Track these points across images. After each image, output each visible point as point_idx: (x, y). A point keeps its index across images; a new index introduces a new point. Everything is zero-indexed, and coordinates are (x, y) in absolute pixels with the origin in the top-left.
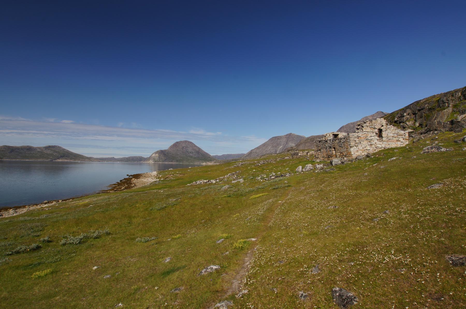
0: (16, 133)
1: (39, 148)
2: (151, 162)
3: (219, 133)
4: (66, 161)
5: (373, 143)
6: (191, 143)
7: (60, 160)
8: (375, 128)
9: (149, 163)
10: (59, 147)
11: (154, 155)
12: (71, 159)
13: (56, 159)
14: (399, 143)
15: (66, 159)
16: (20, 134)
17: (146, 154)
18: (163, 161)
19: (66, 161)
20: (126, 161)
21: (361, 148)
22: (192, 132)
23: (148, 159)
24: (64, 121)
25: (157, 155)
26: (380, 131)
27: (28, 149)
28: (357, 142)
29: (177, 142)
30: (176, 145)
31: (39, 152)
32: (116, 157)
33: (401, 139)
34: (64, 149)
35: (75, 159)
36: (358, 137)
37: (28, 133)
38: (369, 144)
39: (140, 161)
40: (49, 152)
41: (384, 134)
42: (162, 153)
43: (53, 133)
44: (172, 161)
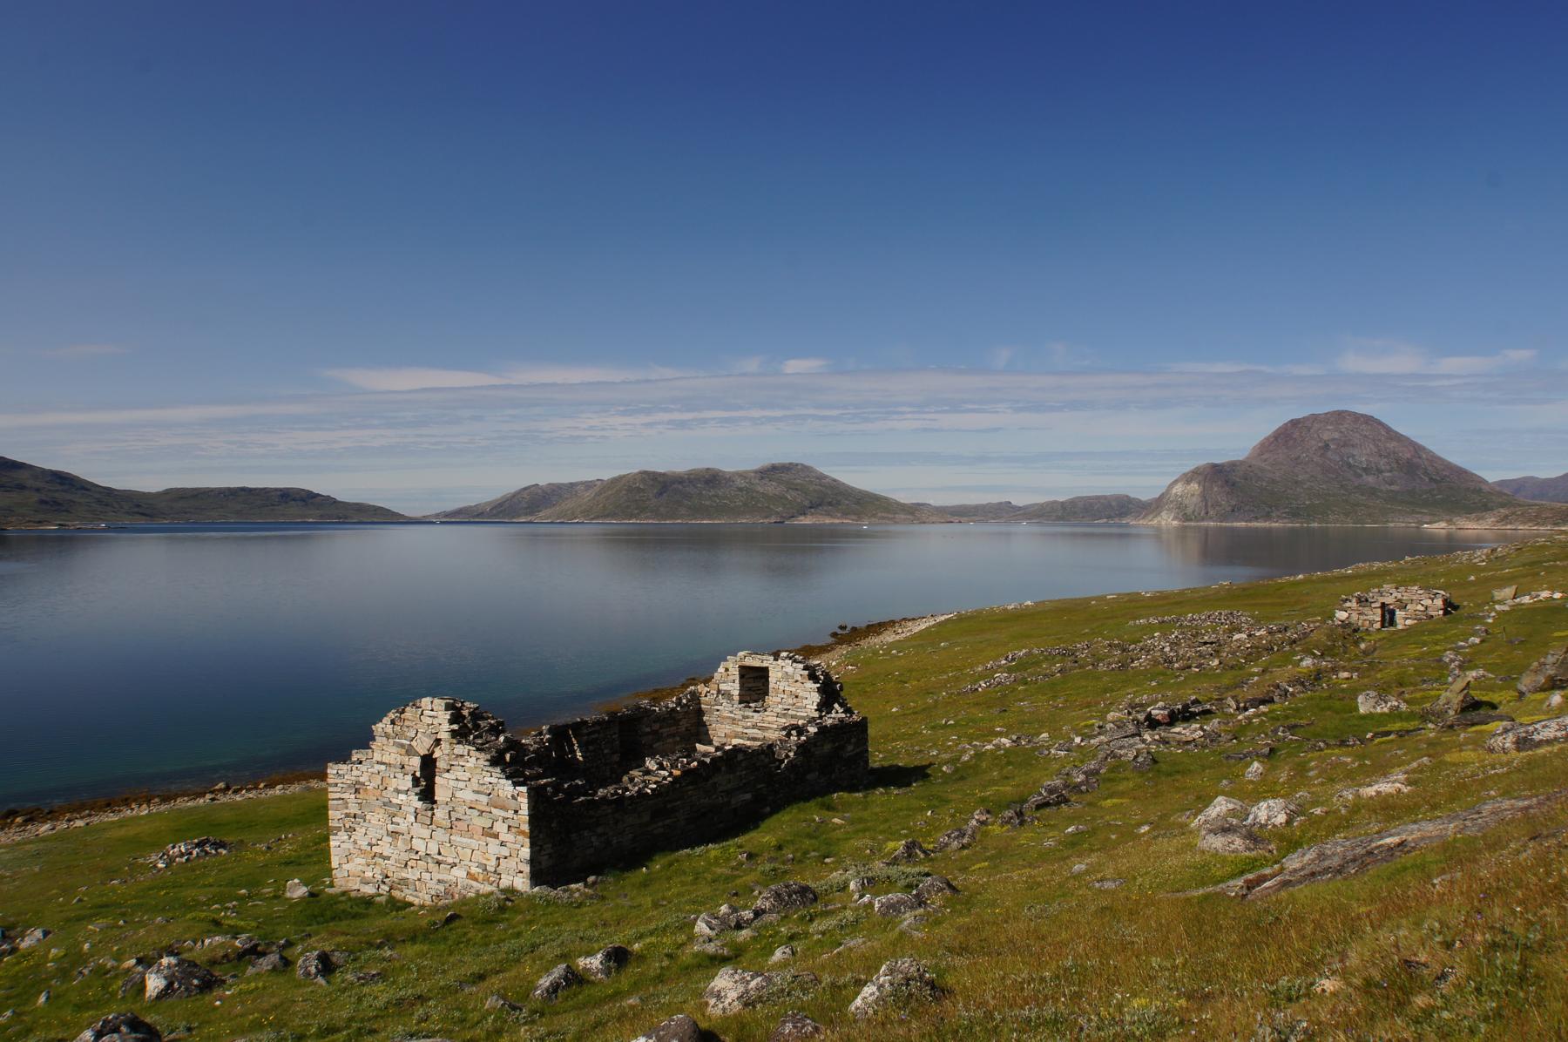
0: (670, 422)
1: (742, 475)
2: (1168, 520)
3: (1520, 356)
4: (828, 521)
5: (403, 827)
6: (1369, 420)
7: (806, 521)
8: (410, 751)
9: (1158, 529)
10: (806, 468)
11: (1178, 489)
12: (845, 514)
13: (797, 515)
14: (494, 847)
15: (829, 514)
16: (682, 425)
17: (1144, 487)
18: (1223, 518)
19: (828, 521)
20: (1059, 518)
21: (363, 844)
22: (1353, 363)
23: (1154, 507)
24: (794, 366)
25: (1194, 486)
26: (428, 763)
27: (707, 482)
28: (354, 809)
29: (1294, 423)
30: (1289, 434)
31: (741, 489)
32: (1019, 500)
33: (500, 827)
34: (822, 477)
35: (859, 515)
36: (357, 788)
37: (704, 421)
38: (391, 828)
39: (1122, 515)
40: (771, 488)
41: (443, 786)
42: (1218, 476)
43: (779, 413)
44: (1267, 517)
